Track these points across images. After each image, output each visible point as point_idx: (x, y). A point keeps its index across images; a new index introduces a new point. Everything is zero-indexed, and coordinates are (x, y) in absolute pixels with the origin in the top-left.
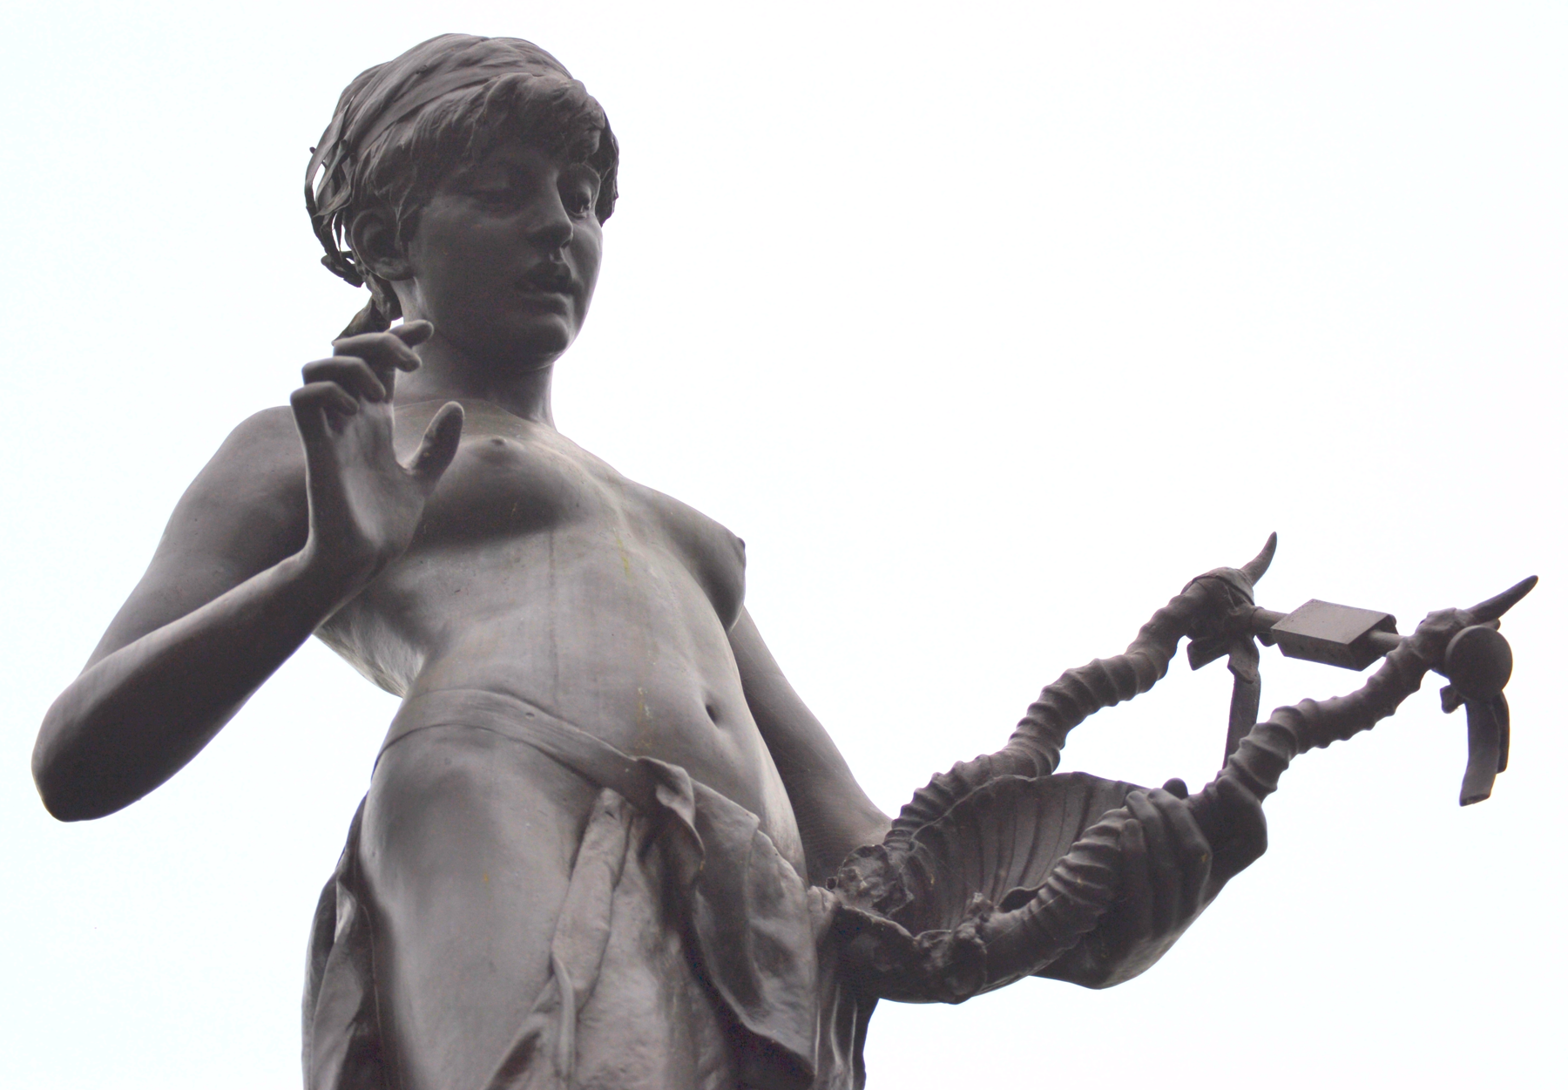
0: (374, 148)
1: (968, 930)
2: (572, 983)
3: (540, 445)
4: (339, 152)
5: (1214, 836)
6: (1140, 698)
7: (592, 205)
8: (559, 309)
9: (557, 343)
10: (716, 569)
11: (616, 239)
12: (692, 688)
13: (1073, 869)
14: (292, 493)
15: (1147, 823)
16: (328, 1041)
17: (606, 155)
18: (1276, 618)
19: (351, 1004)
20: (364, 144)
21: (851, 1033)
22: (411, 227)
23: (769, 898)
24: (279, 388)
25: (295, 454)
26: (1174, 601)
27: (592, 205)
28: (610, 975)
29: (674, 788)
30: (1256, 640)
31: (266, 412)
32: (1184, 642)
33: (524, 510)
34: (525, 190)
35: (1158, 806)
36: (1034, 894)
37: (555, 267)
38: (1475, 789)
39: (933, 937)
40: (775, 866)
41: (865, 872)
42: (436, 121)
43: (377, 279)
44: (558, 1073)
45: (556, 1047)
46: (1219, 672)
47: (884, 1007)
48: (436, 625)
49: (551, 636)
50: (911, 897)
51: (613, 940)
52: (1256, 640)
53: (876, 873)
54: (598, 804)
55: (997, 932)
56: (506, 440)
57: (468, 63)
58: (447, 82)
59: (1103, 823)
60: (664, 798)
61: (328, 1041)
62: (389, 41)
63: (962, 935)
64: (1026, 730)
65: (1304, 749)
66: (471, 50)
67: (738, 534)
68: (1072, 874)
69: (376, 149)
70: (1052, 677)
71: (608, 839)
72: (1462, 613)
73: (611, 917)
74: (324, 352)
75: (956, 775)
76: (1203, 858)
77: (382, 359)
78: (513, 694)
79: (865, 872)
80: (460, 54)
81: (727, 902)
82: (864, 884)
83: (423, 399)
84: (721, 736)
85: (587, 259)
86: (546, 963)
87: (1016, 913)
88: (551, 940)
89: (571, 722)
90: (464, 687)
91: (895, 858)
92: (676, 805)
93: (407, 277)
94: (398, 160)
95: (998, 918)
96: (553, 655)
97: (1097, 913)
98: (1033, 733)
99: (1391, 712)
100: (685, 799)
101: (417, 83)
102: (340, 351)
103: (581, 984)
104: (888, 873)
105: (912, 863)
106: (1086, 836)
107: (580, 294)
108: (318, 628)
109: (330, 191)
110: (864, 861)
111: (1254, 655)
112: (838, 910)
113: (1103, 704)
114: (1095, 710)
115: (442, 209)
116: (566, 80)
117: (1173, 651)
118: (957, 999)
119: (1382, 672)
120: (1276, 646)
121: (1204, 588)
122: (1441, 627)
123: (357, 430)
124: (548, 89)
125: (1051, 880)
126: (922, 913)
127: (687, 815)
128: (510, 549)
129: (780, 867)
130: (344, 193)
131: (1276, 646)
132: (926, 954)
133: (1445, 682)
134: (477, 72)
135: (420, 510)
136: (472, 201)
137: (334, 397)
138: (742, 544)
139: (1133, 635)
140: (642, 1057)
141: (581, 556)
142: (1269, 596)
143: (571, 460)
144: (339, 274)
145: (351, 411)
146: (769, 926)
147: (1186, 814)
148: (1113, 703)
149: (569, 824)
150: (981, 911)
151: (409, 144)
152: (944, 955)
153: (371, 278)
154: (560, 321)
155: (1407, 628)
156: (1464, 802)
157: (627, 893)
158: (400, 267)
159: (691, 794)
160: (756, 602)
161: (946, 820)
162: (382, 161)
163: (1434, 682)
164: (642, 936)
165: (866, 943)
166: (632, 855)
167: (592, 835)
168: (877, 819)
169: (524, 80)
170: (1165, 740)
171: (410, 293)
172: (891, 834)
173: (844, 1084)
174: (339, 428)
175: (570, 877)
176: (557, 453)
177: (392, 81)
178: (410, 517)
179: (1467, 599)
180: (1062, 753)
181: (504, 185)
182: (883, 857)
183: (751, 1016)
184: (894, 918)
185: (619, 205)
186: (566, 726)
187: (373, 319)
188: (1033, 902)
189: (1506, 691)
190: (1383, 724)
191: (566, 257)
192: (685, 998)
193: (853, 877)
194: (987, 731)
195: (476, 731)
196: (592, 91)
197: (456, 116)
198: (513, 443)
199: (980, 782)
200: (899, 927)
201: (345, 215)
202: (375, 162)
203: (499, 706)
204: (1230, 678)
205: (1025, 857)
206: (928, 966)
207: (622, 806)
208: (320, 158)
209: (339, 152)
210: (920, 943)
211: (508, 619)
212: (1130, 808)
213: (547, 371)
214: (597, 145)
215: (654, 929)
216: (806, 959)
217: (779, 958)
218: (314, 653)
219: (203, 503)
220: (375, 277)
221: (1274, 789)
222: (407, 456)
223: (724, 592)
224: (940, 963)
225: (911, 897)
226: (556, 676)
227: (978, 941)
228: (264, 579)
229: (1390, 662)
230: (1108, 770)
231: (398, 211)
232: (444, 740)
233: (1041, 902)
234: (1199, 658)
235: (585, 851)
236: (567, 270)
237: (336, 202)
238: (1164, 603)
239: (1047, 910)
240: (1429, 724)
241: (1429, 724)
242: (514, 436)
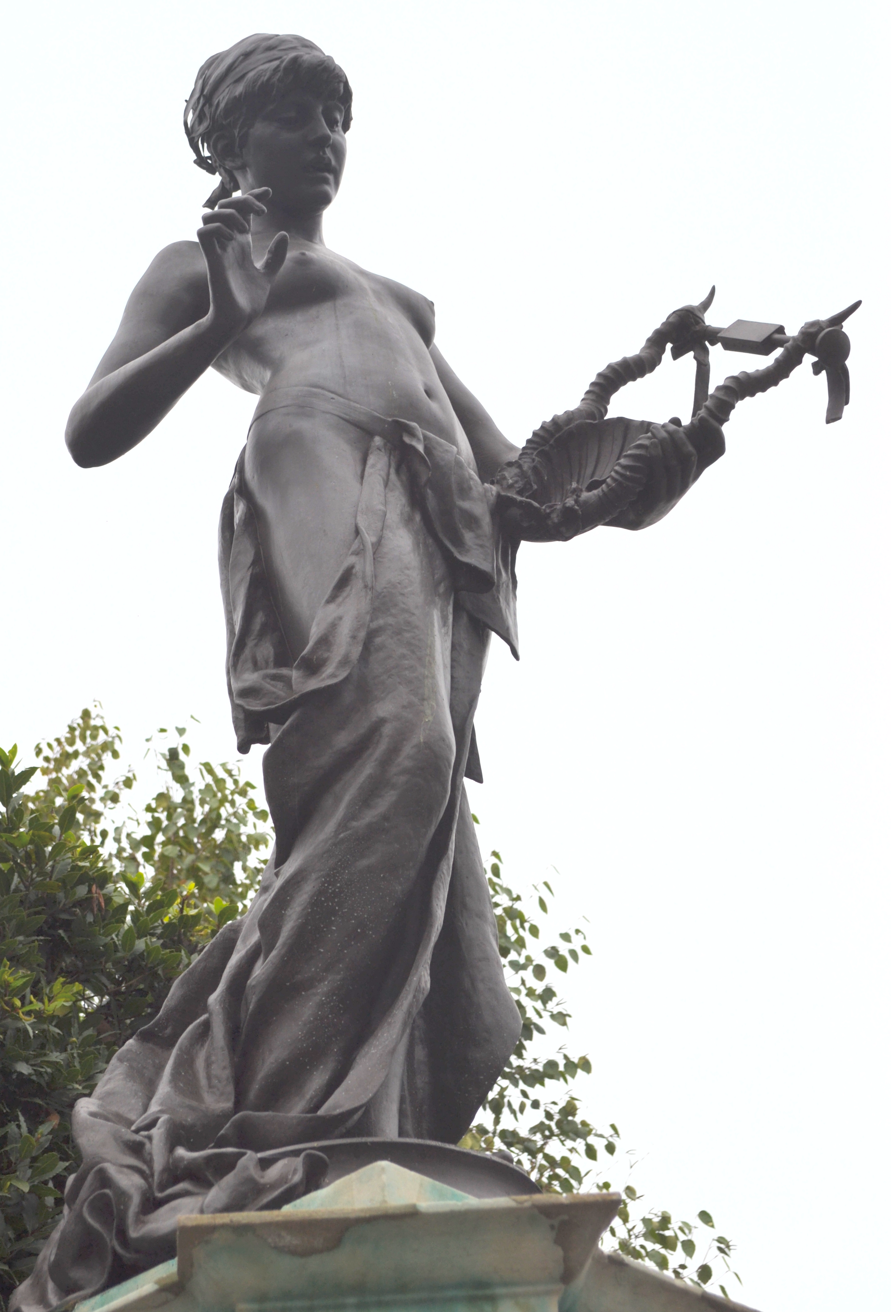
0: (221, 97)
1: (570, 502)
2: (370, 539)
5: (696, 446)
6: (648, 376)
7: (340, 124)
8: (326, 181)
9: (326, 200)
10: (420, 316)
11: (353, 140)
12: (417, 382)
13: (624, 467)
15: (662, 441)
16: (238, 576)
17: (346, 97)
18: (719, 330)
19: (248, 557)
21: (509, 561)
23: (465, 490)
25: (202, 265)
26: (663, 324)
27: (340, 124)
28: (388, 534)
29: (412, 433)
30: (707, 343)
32: (669, 346)
33: (318, 288)
35: (667, 432)
36: (604, 481)
38: (834, 414)
39: (551, 507)
40: (467, 474)
41: (510, 475)
42: (255, 81)
43: (226, 170)
44: (366, 587)
45: (364, 572)
46: (689, 360)
47: (524, 546)
48: (276, 354)
49: (340, 356)
50: (535, 487)
51: (388, 516)
52: (707, 343)
53: (516, 475)
54: (373, 444)
55: (586, 502)
56: (307, 253)
57: (270, 48)
59: (638, 442)
60: (407, 439)
61: (238, 576)
62: (225, 39)
63: (568, 505)
64: (590, 396)
65: (742, 398)
66: (271, 42)
67: (430, 299)
68: (616, 471)
69: (223, 98)
70: (602, 367)
71: (378, 462)
72: (823, 322)
73: (386, 503)
75: (555, 421)
76: (693, 458)
78: (323, 388)
79: (510, 475)
80: (265, 44)
81: (444, 494)
82: (510, 481)
84: (434, 406)
85: (339, 153)
86: (354, 529)
87: (595, 492)
88: (356, 517)
89: (355, 402)
90: (296, 386)
91: (526, 467)
92: (414, 443)
93: (243, 168)
94: (235, 104)
95: (585, 495)
97: (637, 490)
98: (594, 397)
99: (787, 376)
100: (419, 439)
101: (242, 62)
103: (374, 539)
104: (523, 474)
105: (535, 469)
106: (630, 449)
107: (337, 173)
110: (509, 469)
111: (706, 351)
112: (499, 496)
113: (629, 380)
114: (625, 383)
115: (261, 129)
117: (663, 351)
118: (566, 539)
119: (782, 355)
120: (719, 345)
121: (680, 316)
122: (812, 330)
123: (233, 249)
125: (613, 474)
126: (542, 495)
127: (420, 448)
128: (313, 311)
129: (469, 474)
130: (205, 124)
131: (719, 345)
132: (548, 516)
133: (816, 359)
135: (268, 293)
136: (274, 122)
137: (217, 233)
139: (643, 343)
140: (408, 576)
141: (351, 313)
142: (713, 319)
145: (231, 238)
146: (466, 505)
147: (682, 435)
148: (634, 379)
149: (358, 456)
150: (577, 492)
151: (240, 95)
152: (558, 516)
153: (222, 170)
154: (327, 188)
155: (792, 331)
156: (828, 422)
157: (392, 490)
158: (239, 163)
159: (421, 437)
161: (551, 445)
162: (227, 104)
163: (809, 359)
164: (402, 514)
165: (515, 512)
166: (392, 471)
167: (371, 460)
168: (512, 448)
169: (301, 56)
170: (662, 398)
171: (245, 177)
172: (521, 455)
173: (508, 586)
174: (224, 248)
175: (362, 484)
177: (229, 61)
178: (263, 296)
179: (824, 315)
180: (609, 407)
182: (520, 466)
183: (459, 552)
184: (527, 498)
185: (353, 124)
186: (352, 403)
187: (223, 192)
188: (604, 486)
189: (847, 362)
190: (783, 383)
191: (329, 153)
192: (426, 546)
193: (504, 478)
194: (568, 398)
195: (304, 408)
196: (338, 61)
197: (266, 78)
199: (567, 425)
200: (533, 502)
201: (206, 137)
202: (222, 105)
203: (315, 395)
204: (695, 363)
205: (594, 463)
206: (550, 522)
207: (385, 445)
210: (545, 510)
211: (313, 349)
212: (653, 433)
213: (320, 216)
215: (407, 509)
216: (486, 521)
217: (472, 521)
218: (210, 373)
219: (144, 294)
221: (727, 420)
224: (556, 520)
225: (535, 487)
226: (345, 377)
227: (576, 507)
228: (187, 332)
229: (787, 349)
230: (636, 414)
231: (236, 132)
232: (288, 414)
233: (608, 485)
234: (676, 354)
235: (367, 469)
236: (330, 160)
237: (202, 129)
238: (658, 326)
239: (612, 490)
240: (807, 383)
241: (807, 383)
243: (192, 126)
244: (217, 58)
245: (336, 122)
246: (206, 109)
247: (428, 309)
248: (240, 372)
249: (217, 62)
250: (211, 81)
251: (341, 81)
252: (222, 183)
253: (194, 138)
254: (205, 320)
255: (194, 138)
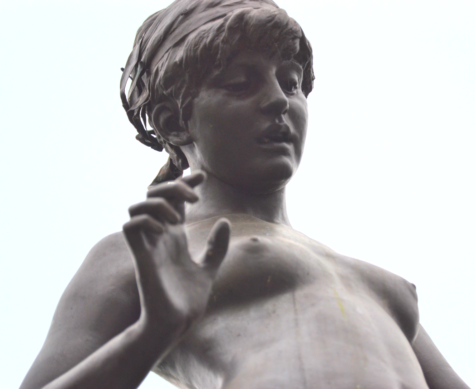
3: (281, 238)
4: (139, 69)
7: (299, 86)
8: (285, 152)
9: (286, 173)
10: (402, 310)
11: (318, 107)
14: (129, 286)
17: (305, 54)
20: (154, 63)
22: (188, 112)
24: (118, 220)
25: (128, 261)
31: (91, 252)
33: (270, 280)
34: (256, 81)
37: (280, 127)
42: (197, 44)
49: (299, 358)
58: (201, 19)
67: (411, 280)
69: (162, 65)
74: (141, 198)
77: (176, 198)
83: (207, 217)
85: (299, 119)
93: (190, 142)
94: (176, 71)
96: (302, 370)
102: (150, 195)
108: (155, 366)
109: (136, 94)
115: (206, 98)
116: (275, 9)
123: (165, 243)
124: (264, 16)
128: (269, 305)
130: (145, 94)
134: (219, 10)
138: (414, 286)
141: (313, 305)
143: (301, 246)
144: (148, 144)
145: (160, 232)
151: (181, 61)
153: (167, 146)
154: (286, 160)
158: (184, 137)
160: (426, 321)
162: (166, 72)
169: (248, 12)
171: (192, 152)
174: (153, 243)
176: (292, 242)
177: (167, 21)
178: (204, 292)
181: (242, 79)
185: (316, 84)
187: (172, 171)
191: (286, 120)
197: (209, 40)
198: (264, 239)
202: (161, 73)
208: (127, 74)
209: (139, 69)
213: (282, 191)
214: (298, 48)
219: (75, 296)
220: (170, 145)
222: (198, 253)
223: (406, 320)
228: (117, 342)
231: (179, 102)
236: (288, 128)
237: (140, 101)
242: (264, 234)
243: (132, 97)
244: (154, 19)
245: (294, 84)
246: (145, 79)
247: (408, 293)
248: (191, 382)
249: (155, 21)
250: (149, 46)
251: (295, 38)
252: (171, 160)
253: (133, 111)
254: (137, 327)
255: (133, 111)
